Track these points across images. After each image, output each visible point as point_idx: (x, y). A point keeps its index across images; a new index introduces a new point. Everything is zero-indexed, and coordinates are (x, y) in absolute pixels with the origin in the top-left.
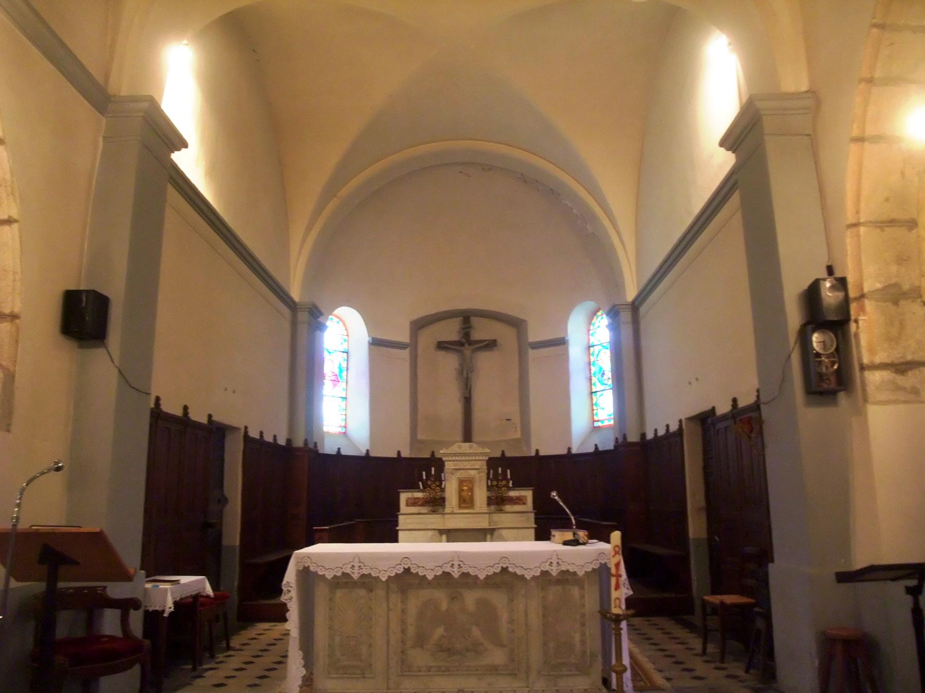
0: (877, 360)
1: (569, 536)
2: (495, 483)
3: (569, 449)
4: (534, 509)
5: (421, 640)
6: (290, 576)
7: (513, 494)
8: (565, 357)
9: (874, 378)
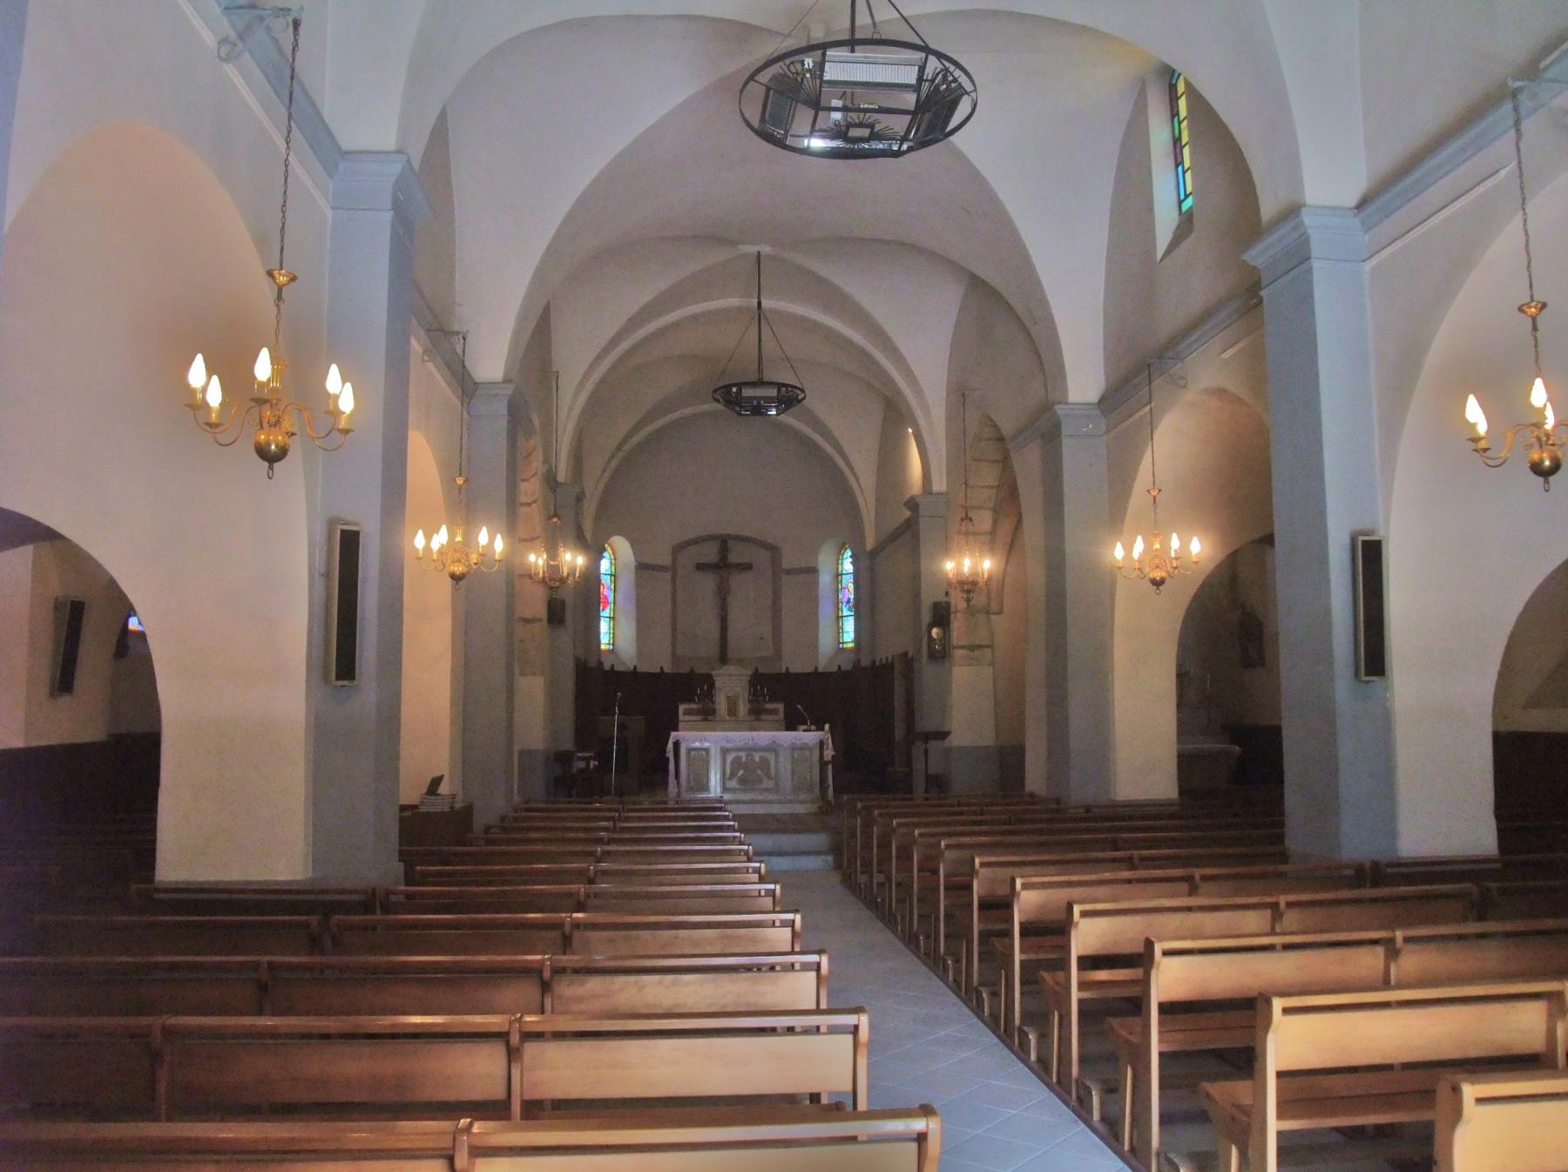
0: (961, 643)
1: (805, 727)
2: (754, 698)
3: (816, 668)
4: (785, 718)
5: (733, 775)
6: (670, 745)
7: (769, 706)
8: (816, 583)
9: (959, 653)
